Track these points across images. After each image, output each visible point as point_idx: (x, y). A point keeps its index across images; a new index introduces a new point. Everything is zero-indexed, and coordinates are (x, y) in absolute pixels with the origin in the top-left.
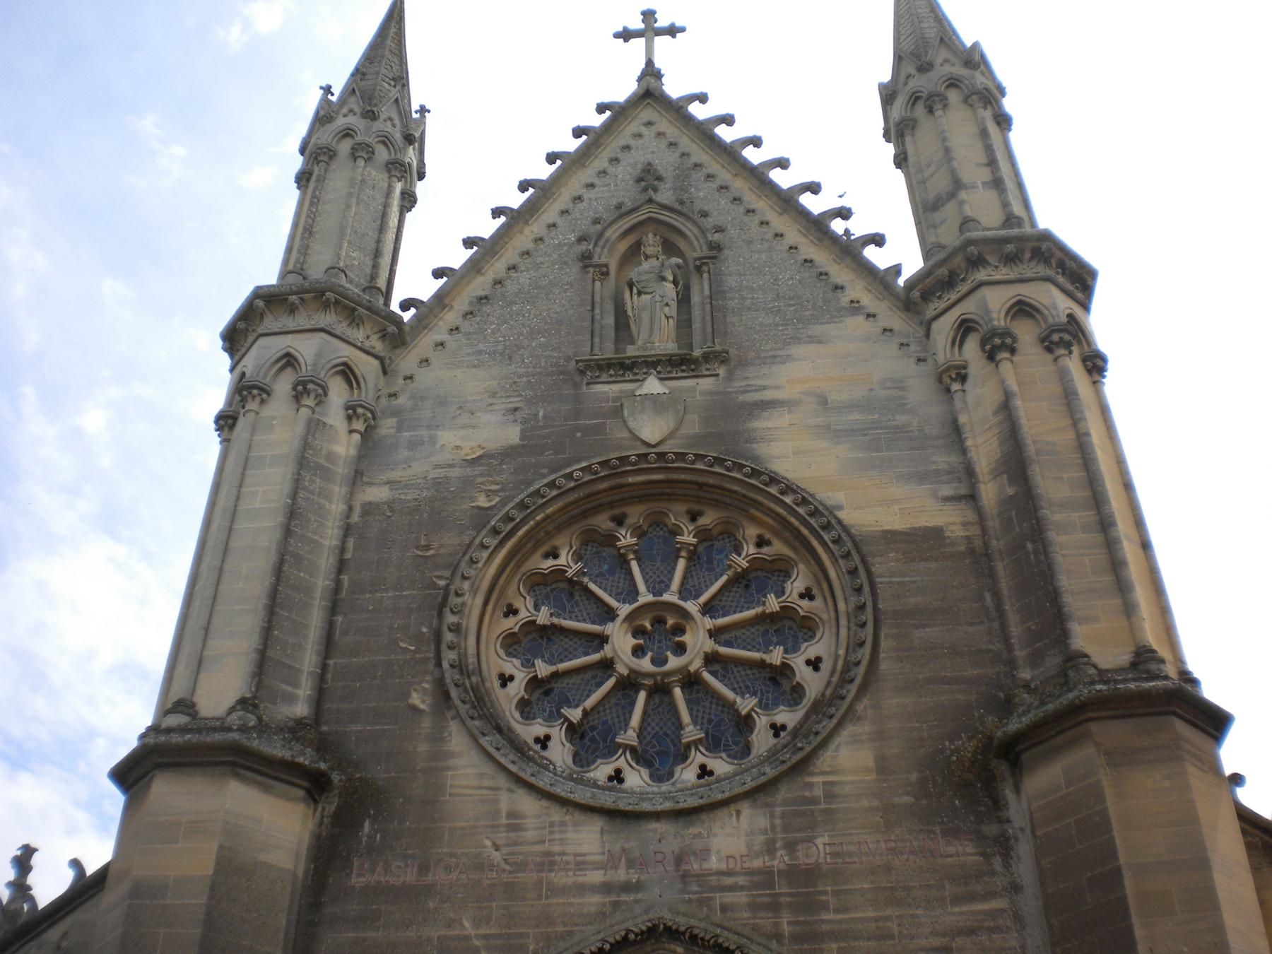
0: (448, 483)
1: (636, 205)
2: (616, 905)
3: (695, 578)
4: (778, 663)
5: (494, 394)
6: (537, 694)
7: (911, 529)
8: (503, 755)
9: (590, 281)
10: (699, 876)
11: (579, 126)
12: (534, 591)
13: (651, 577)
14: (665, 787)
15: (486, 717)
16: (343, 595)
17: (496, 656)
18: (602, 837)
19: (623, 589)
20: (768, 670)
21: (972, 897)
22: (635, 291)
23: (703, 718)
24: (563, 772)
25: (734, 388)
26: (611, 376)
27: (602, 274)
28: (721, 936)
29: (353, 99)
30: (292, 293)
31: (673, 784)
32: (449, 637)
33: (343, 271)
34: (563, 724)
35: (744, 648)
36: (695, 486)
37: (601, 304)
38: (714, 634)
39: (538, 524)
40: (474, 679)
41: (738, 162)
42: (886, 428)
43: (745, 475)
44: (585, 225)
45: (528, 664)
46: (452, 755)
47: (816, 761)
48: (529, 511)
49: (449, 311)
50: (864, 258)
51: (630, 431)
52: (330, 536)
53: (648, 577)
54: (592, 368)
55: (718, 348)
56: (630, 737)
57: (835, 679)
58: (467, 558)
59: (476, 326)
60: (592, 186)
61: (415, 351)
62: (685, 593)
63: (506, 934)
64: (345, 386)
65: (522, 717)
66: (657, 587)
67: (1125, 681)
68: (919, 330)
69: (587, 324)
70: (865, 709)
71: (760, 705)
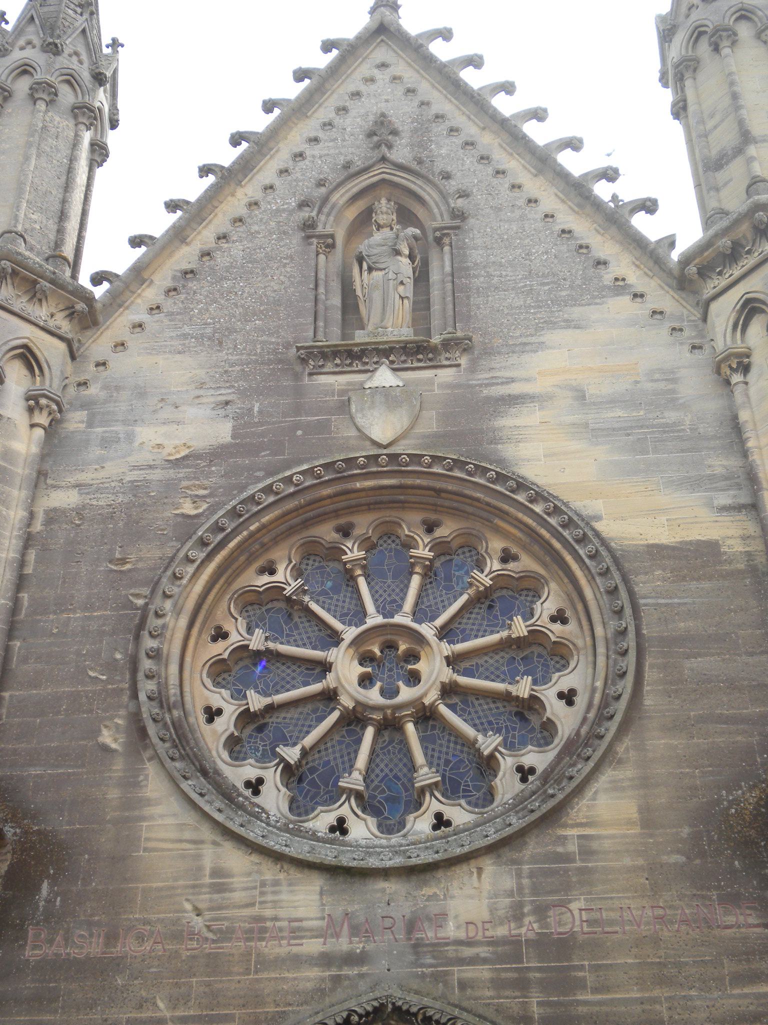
0: (148, 487)
1: (367, 164)
3: (431, 597)
4: (526, 696)
5: (201, 385)
6: (248, 731)
7: (681, 542)
8: (208, 802)
9: (313, 255)
11: (300, 68)
12: (247, 611)
13: (381, 596)
14: (395, 839)
15: (190, 758)
16: (22, 616)
17: (202, 687)
18: (321, 899)
19: (349, 609)
20: (513, 703)
23: (439, 758)
24: (277, 822)
25: (475, 380)
26: (337, 365)
27: (327, 246)
28: (458, 1018)
29: (31, 29)
31: (404, 836)
32: (147, 664)
33: (22, 236)
34: (278, 765)
35: (487, 678)
36: (432, 493)
37: (326, 282)
38: (452, 661)
39: (252, 535)
40: (176, 713)
41: (486, 113)
42: (653, 426)
43: (488, 480)
44: (308, 188)
45: (238, 695)
46: (148, 802)
47: (569, 810)
48: (241, 520)
49: (149, 286)
50: (631, 227)
51: (358, 429)
53: (377, 596)
54: (316, 356)
55: (459, 334)
56: (354, 780)
57: (591, 715)
58: (169, 573)
59: (181, 305)
60: (315, 140)
61: (109, 333)
62: (419, 614)
63: (207, 1015)
64: (24, 371)
65: (230, 757)
66: (389, 607)
68: (696, 312)
69: (310, 305)
70: (627, 750)
71: (505, 744)
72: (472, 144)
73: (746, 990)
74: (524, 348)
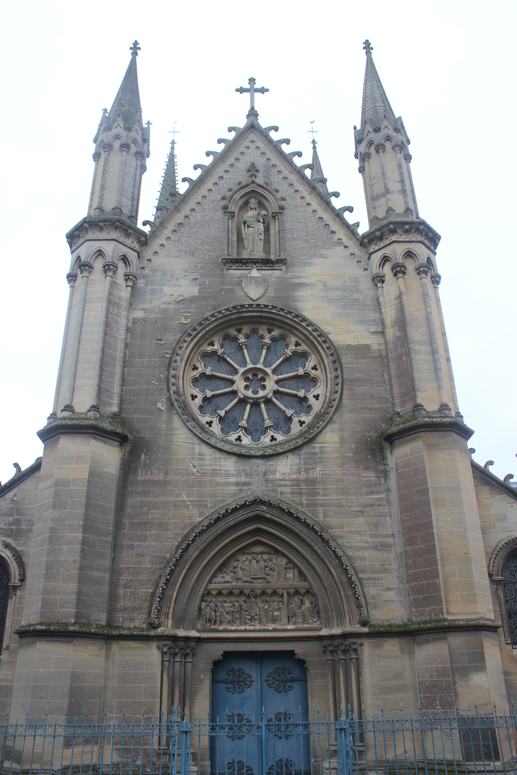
2: (241, 490)
6: (206, 403)
9: (227, 220)
10: (272, 480)
16: (127, 359)
21: (372, 493)
22: (246, 225)
30: (101, 222)
32: (172, 380)
34: (217, 416)
37: (232, 230)
38: (277, 382)
40: (183, 398)
43: (292, 316)
46: (175, 429)
51: (245, 293)
52: (121, 334)
54: (229, 263)
55: (282, 257)
56: (244, 423)
57: (325, 405)
58: (178, 346)
62: (265, 364)
64: (124, 265)
66: (255, 361)
67: (435, 417)
69: (226, 240)
70: (336, 418)
72: (286, 178)
73: (369, 497)
74: (305, 264)
